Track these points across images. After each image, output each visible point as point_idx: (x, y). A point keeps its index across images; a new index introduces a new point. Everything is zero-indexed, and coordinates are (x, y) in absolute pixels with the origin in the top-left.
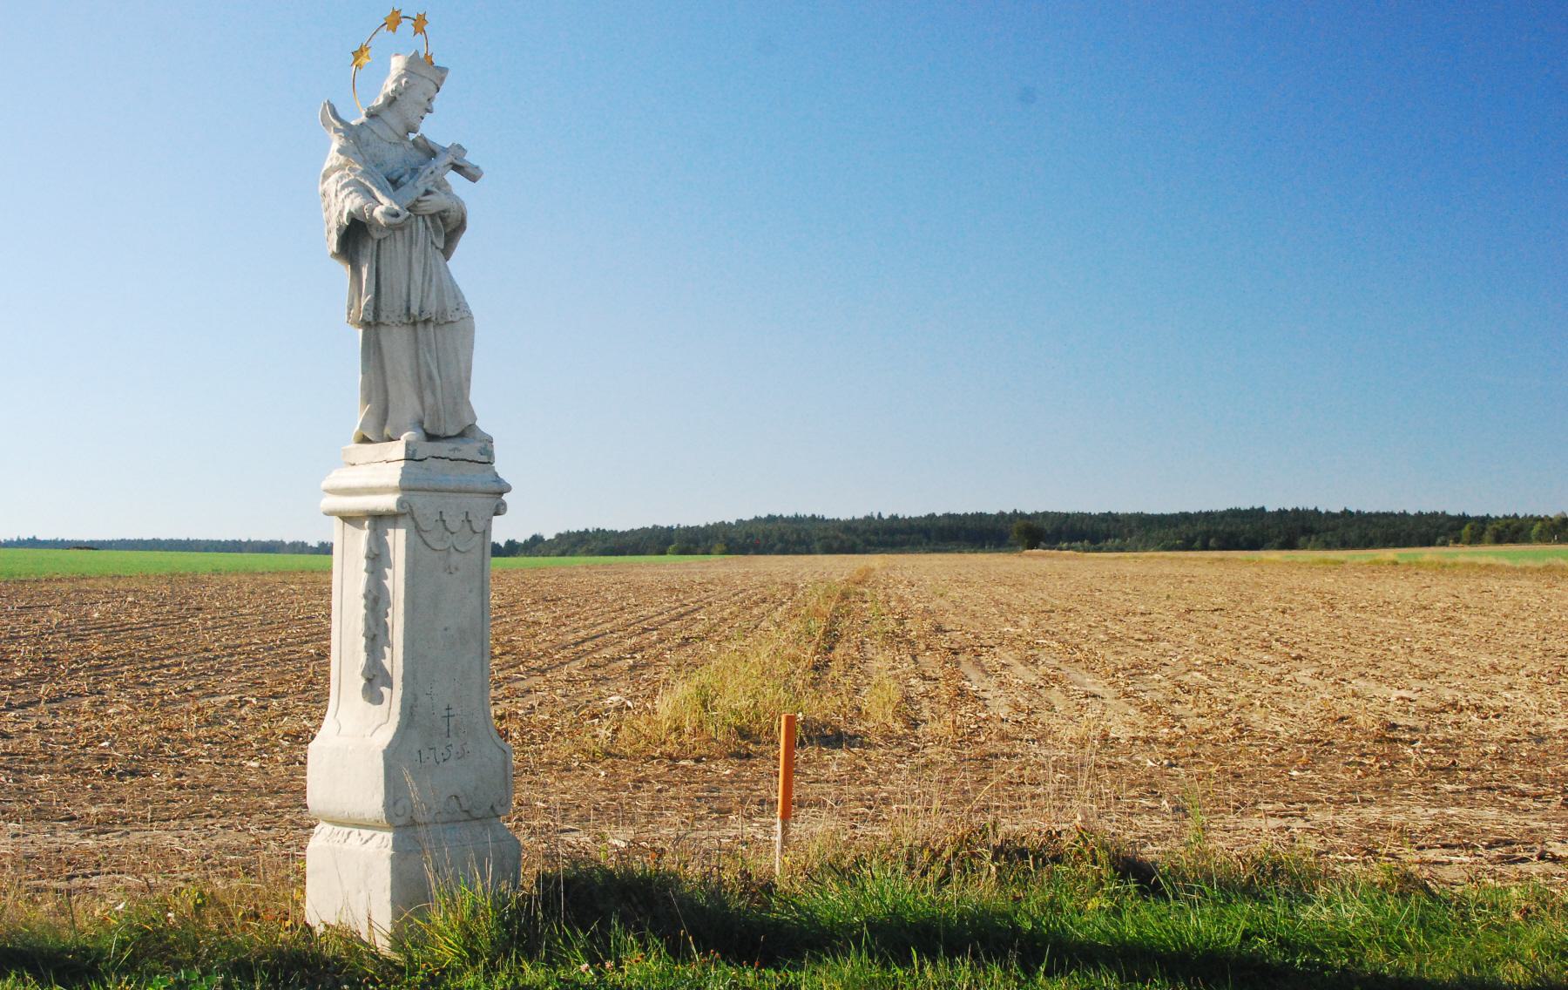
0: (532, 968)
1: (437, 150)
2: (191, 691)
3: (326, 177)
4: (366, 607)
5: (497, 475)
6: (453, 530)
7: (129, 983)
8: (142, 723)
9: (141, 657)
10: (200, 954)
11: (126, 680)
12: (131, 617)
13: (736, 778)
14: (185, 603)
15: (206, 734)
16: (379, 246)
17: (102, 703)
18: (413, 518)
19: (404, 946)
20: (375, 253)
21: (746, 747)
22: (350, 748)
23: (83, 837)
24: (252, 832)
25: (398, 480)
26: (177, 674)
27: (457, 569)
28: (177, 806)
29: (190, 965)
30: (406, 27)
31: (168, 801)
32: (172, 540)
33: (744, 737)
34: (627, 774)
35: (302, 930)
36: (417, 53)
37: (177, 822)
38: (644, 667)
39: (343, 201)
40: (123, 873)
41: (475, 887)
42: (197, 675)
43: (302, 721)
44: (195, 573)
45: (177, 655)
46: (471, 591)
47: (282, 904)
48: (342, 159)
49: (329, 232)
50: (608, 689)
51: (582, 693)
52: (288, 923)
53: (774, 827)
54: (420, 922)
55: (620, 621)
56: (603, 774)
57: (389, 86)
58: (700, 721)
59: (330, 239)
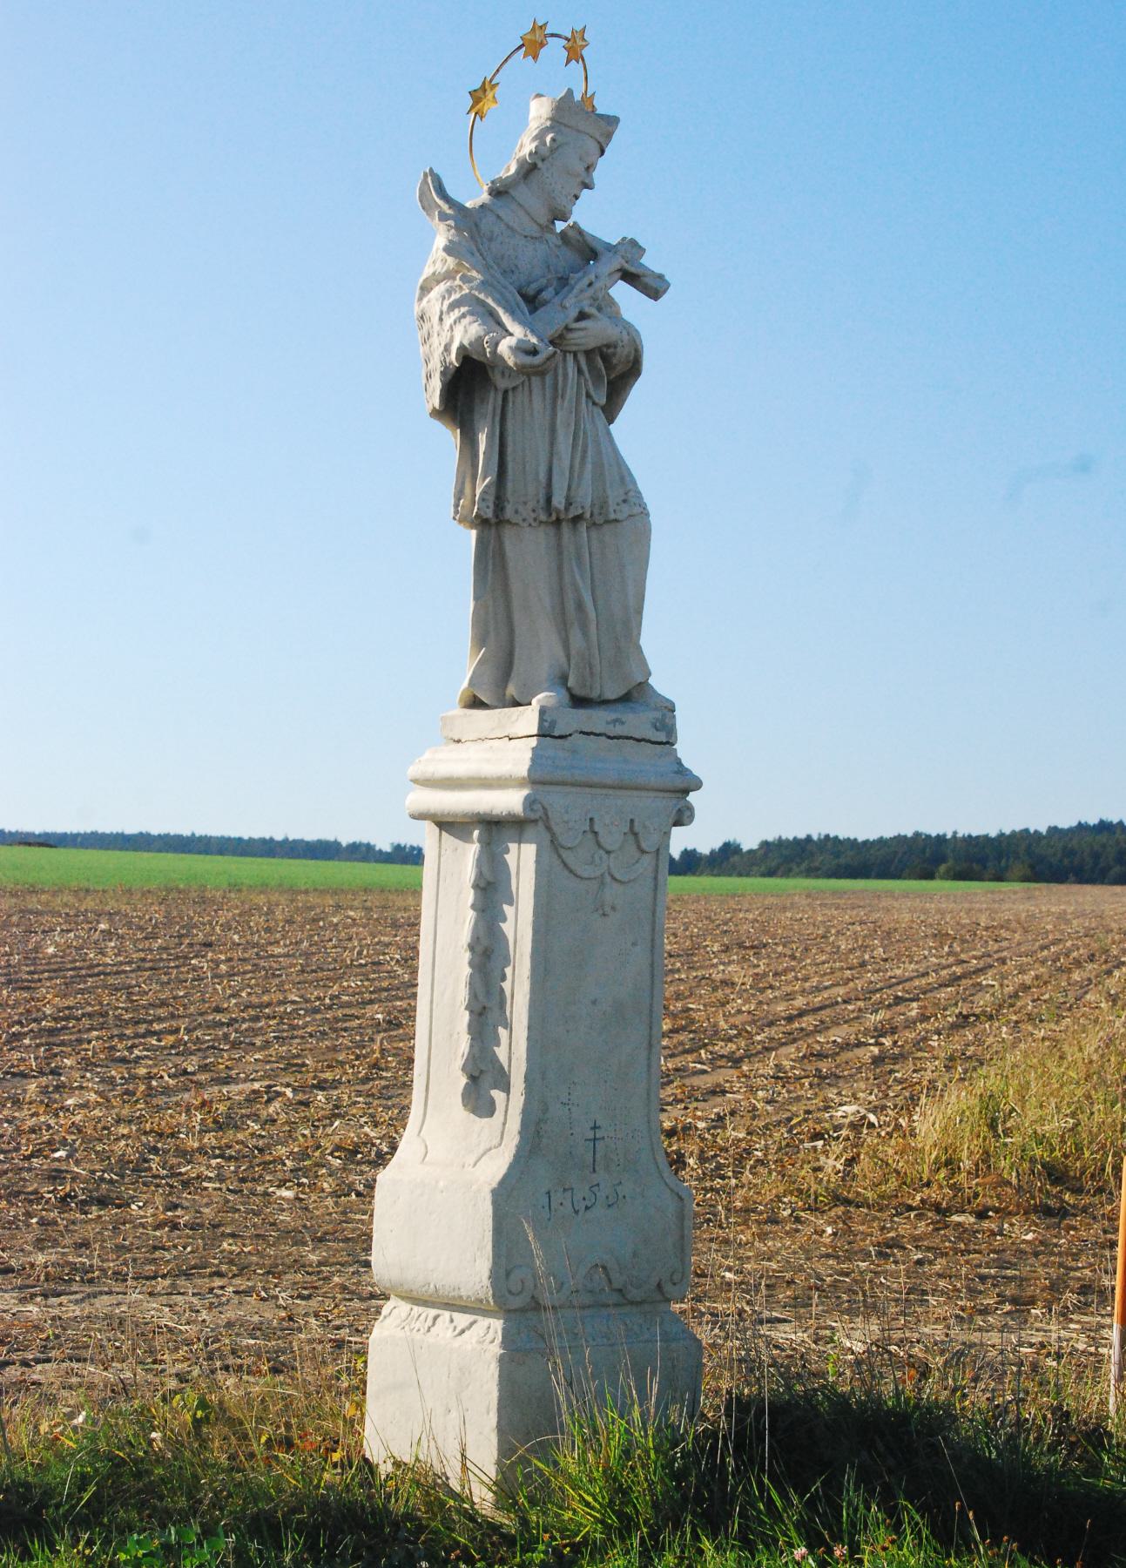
0: (717, 1548)
1: (599, 248)
2: (193, 1074)
3: (425, 289)
4: (471, 964)
5: (679, 763)
6: (609, 848)
7: (90, 1543)
8: (118, 1121)
9: (118, 1018)
10: (200, 1502)
11: (95, 1053)
12: (104, 954)
13: (1042, 1248)
14: (186, 936)
15: (214, 1142)
16: (505, 399)
17: (57, 1088)
18: (548, 828)
19: (516, 1503)
20: (499, 411)
21: (1058, 1197)
22: (441, 1184)
23: (23, 1301)
24: (281, 1302)
25: (527, 767)
26: (172, 1047)
27: (613, 908)
28: (168, 1256)
29: (183, 1519)
30: (554, 51)
31: (155, 1248)
32: (167, 836)
33: (1056, 1181)
34: (869, 1232)
35: (359, 1469)
36: (570, 92)
37: (167, 1282)
38: (895, 1059)
39: (451, 327)
40: (85, 1360)
41: (629, 1414)
42: (202, 1049)
43: (362, 1126)
44: (203, 888)
45: (173, 1016)
46: (634, 944)
47: (327, 1425)
48: (451, 262)
49: (429, 377)
50: (839, 1094)
51: (798, 1099)
52: (336, 1457)
53: (1105, 1333)
54: (541, 1465)
55: (859, 984)
56: (829, 1230)
57: (527, 147)
58: (986, 1152)
59: (430, 389)
